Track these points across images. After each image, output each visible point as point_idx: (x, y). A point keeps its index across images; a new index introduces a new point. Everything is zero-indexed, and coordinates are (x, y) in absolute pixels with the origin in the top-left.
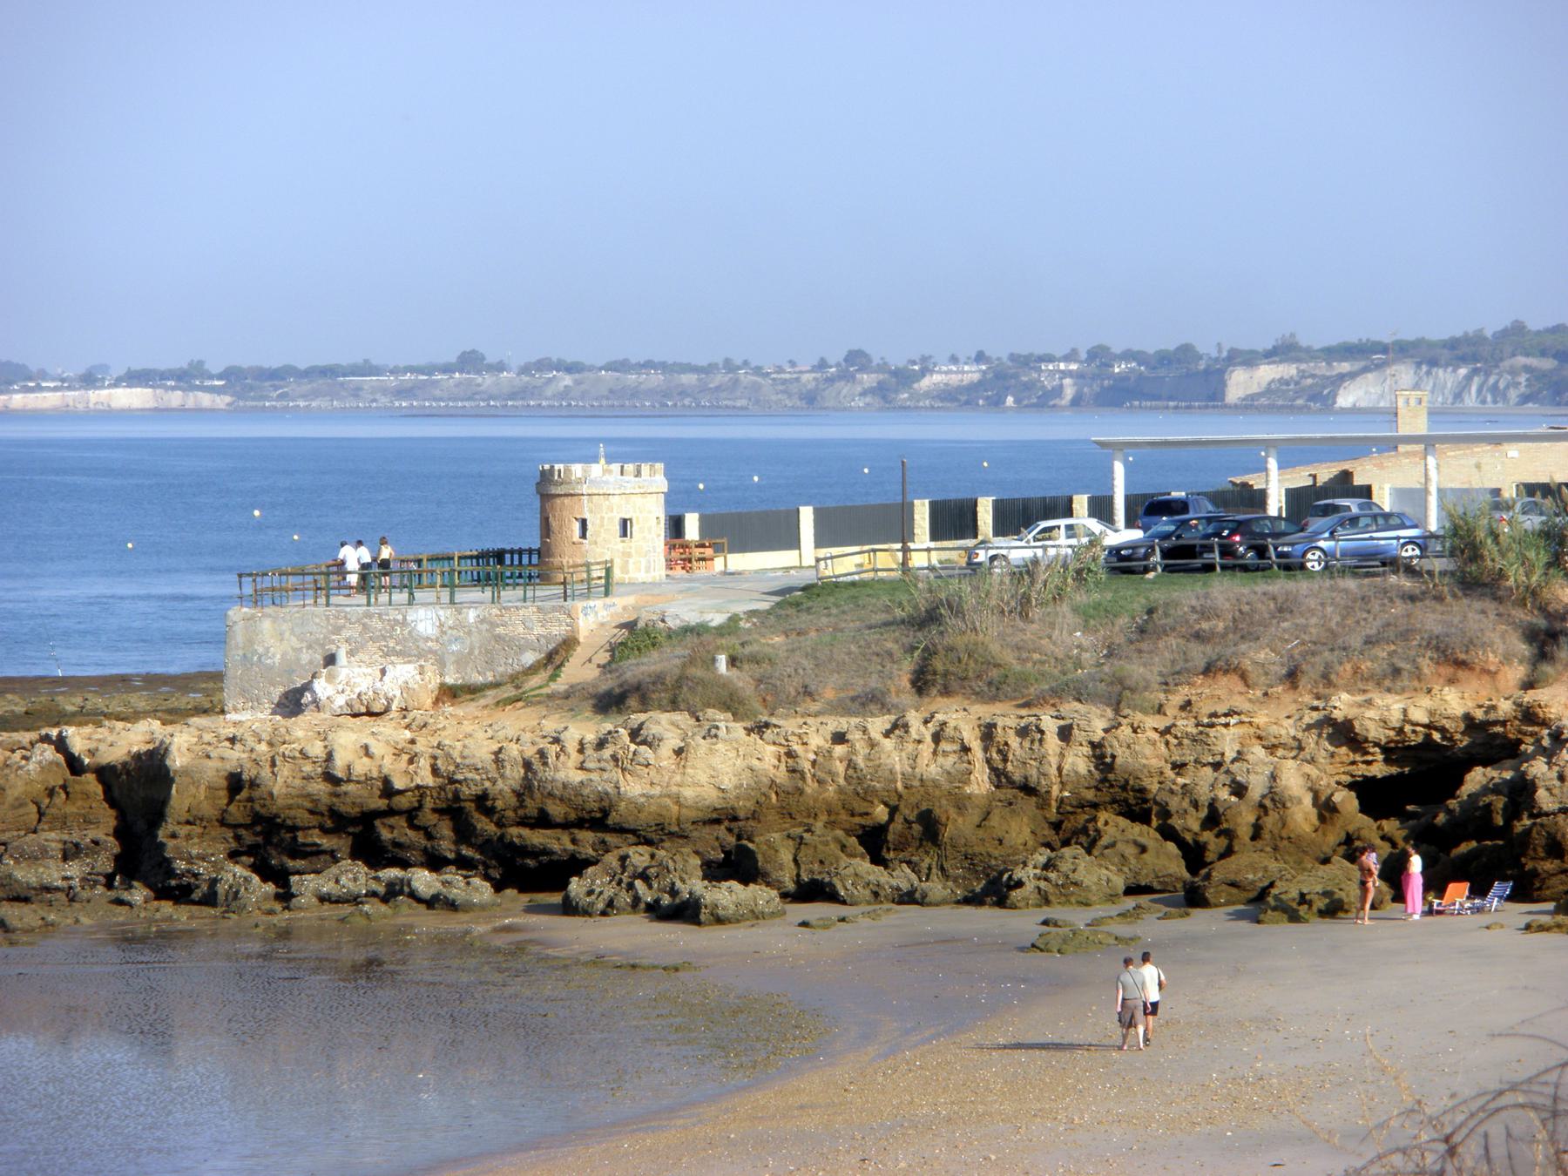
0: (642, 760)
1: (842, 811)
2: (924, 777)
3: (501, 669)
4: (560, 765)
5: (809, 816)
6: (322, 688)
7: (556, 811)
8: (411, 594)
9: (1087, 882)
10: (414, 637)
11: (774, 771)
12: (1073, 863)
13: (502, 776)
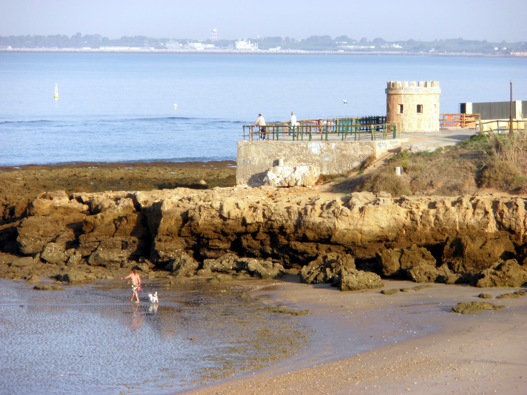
0: (344, 214)
1: (432, 239)
2: (468, 224)
3: (345, 169)
4: (312, 215)
5: (418, 240)
6: (271, 175)
7: (310, 235)
8: (310, 136)
9: (513, 276)
10: (310, 154)
11: (405, 220)
12: (508, 267)
13: (290, 219)
